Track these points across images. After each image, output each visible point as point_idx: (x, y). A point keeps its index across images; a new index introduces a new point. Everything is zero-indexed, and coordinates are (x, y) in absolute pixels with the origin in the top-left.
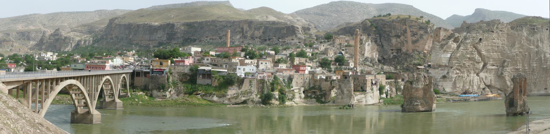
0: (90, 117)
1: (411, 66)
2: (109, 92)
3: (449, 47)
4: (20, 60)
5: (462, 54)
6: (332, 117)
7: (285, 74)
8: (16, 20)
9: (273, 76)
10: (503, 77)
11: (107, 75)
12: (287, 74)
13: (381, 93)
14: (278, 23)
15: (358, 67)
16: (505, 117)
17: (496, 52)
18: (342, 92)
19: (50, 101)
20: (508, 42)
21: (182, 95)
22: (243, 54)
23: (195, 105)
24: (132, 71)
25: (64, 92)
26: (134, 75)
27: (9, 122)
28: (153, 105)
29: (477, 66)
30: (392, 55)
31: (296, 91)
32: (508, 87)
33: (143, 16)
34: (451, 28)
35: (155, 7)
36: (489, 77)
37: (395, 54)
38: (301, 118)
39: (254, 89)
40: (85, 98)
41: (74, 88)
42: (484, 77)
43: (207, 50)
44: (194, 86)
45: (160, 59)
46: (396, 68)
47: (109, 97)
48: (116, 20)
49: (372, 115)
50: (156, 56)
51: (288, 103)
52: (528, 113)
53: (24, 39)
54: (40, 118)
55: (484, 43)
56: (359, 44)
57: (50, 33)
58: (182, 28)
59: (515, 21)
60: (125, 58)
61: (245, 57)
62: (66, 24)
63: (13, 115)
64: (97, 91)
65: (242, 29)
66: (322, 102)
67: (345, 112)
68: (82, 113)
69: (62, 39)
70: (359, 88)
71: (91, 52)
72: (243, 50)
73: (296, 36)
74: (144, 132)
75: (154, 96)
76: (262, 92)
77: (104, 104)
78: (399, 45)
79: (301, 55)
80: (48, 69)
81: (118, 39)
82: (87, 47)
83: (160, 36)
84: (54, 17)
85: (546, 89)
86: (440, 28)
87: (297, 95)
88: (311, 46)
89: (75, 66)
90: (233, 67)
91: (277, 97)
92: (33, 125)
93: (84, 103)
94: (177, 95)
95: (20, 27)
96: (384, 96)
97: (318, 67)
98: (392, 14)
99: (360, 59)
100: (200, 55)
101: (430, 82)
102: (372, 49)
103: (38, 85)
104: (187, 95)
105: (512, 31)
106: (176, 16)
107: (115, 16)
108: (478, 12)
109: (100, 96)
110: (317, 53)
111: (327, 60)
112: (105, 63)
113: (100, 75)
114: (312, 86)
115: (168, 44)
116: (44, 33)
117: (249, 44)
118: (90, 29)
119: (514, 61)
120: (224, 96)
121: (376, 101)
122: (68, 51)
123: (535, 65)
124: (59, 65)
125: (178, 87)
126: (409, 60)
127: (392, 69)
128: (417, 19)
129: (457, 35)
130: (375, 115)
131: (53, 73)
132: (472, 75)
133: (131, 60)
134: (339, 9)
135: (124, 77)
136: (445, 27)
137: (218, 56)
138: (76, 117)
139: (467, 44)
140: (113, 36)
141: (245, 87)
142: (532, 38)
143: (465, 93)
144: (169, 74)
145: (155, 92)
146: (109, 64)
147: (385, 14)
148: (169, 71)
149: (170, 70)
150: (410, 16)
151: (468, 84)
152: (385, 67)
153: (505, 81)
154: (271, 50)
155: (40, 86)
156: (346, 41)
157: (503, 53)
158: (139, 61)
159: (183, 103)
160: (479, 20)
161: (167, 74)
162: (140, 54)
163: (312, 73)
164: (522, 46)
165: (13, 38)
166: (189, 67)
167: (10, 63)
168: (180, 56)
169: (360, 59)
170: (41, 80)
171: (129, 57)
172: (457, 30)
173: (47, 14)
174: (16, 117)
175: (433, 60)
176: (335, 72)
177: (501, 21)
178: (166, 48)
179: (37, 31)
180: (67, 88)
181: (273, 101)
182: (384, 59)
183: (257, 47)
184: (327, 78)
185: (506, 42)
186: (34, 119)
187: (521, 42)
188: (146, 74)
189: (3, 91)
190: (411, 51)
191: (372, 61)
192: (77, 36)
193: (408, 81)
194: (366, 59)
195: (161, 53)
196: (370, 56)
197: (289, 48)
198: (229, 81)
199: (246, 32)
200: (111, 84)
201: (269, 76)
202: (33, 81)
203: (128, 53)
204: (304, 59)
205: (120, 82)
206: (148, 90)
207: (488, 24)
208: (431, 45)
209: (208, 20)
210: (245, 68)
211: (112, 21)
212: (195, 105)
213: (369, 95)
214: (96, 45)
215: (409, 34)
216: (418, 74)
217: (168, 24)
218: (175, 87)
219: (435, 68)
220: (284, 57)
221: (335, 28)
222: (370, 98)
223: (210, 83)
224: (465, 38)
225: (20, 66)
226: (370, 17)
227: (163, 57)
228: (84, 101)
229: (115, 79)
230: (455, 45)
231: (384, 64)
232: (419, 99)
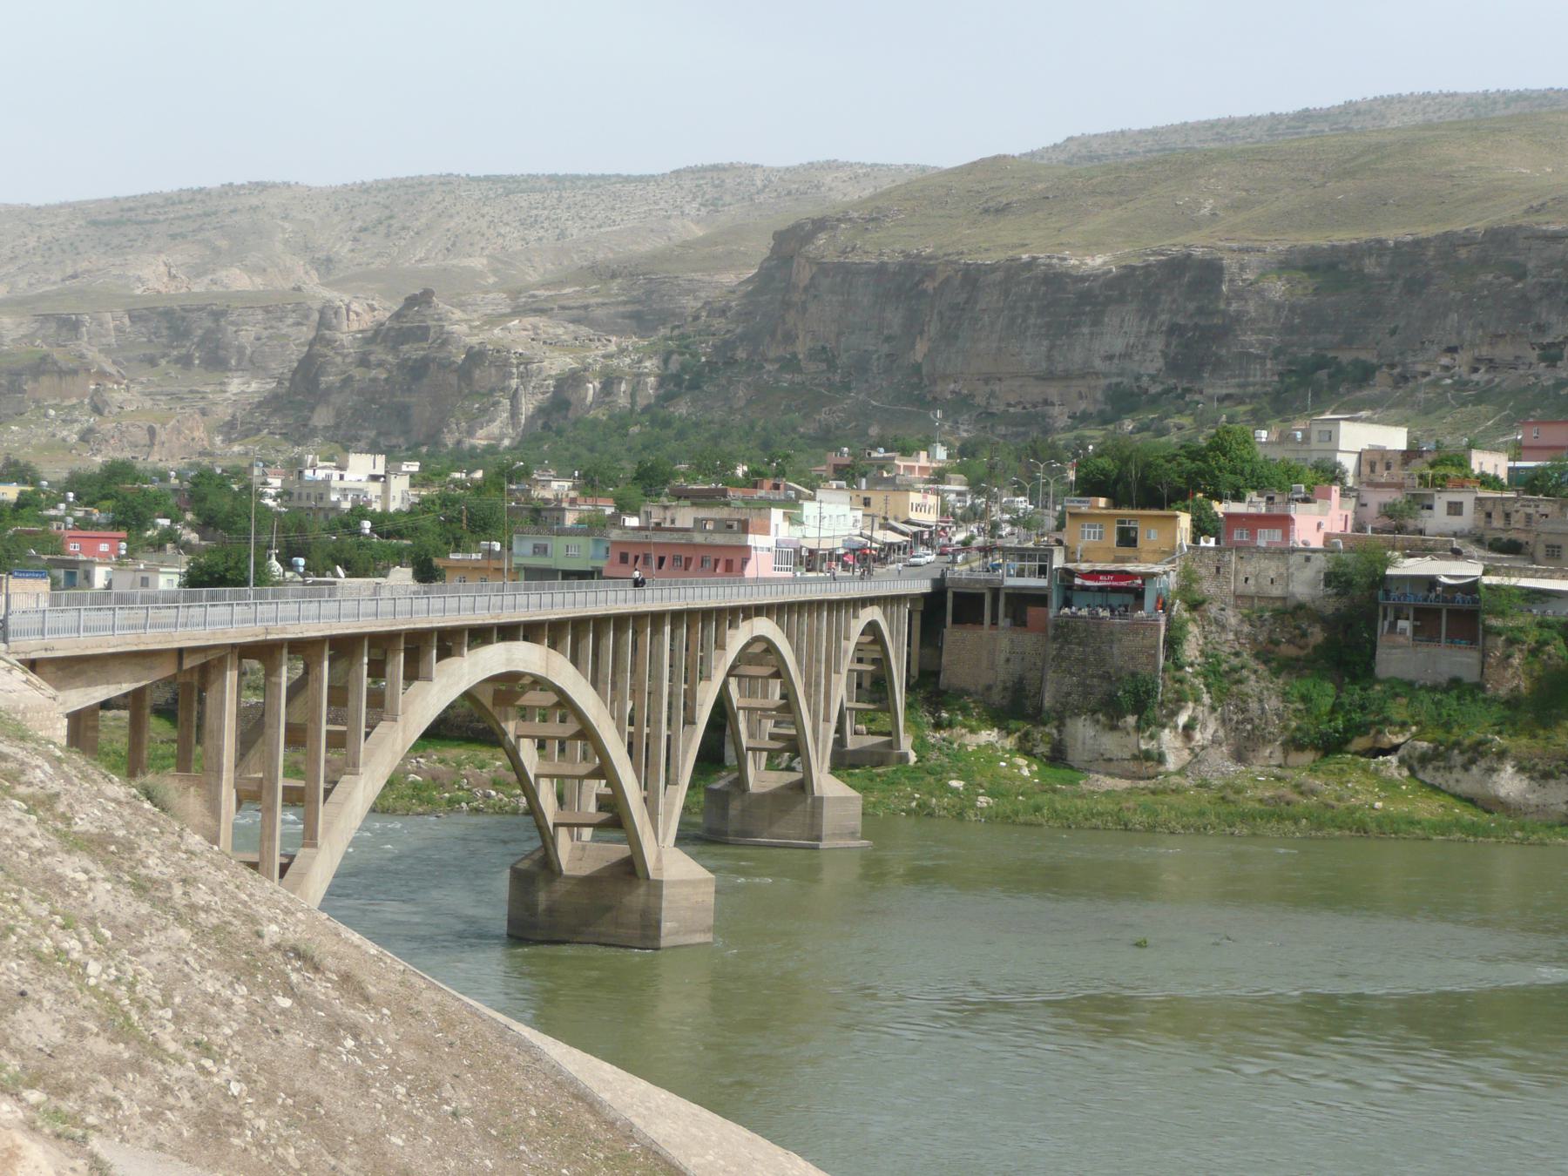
0: (637, 898)
2: (769, 726)
4: (155, 503)
8: (125, 222)
19: (362, 790)
21: (1270, 754)
23: (1362, 829)
24: (925, 587)
25: (464, 726)
26: (939, 611)
27: (71, 944)
28: (1067, 822)
33: (1002, 210)
35: (1084, 141)
40: (605, 770)
41: (533, 698)
44: (1355, 694)
45: (1116, 502)
47: (771, 766)
48: (822, 239)
50: (1090, 486)
53: (185, 362)
54: (297, 908)
57: (367, 321)
58: (1277, 288)
60: (877, 498)
62: (478, 263)
63: (103, 894)
64: (690, 721)
68: (586, 869)
69: (446, 365)
71: (650, 458)
74: (1007, 1007)
75: (1076, 755)
77: (735, 807)
80: (352, 571)
81: (831, 364)
82: (620, 423)
83: (1119, 345)
84: (392, 206)
89: (541, 550)
92: (246, 958)
93: (603, 803)
94: (1239, 756)
95: (154, 275)
100: (1398, 473)
103: (284, 677)
104: (1308, 757)
106: (1236, 207)
107: (816, 213)
109: (711, 756)
112: (745, 527)
113: (706, 614)
115: (1178, 399)
116: (323, 323)
118: (640, 297)
122: (491, 450)
124: (430, 541)
125: (1243, 698)
131: (389, 601)
133: (923, 508)
135: (872, 627)
137: (1529, 483)
138: (542, 899)
140: (802, 347)
144: (1178, 607)
145: (1083, 733)
146: (771, 538)
148: (1184, 590)
149: (1188, 578)
155: (296, 689)
158: (972, 515)
159: (1277, 811)
161: (1164, 605)
165: (107, 350)
166: (1320, 563)
167: (84, 524)
168: (1258, 487)
170: (301, 648)
171: (908, 487)
173: (348, 189)
174: (128, 907)
178: (1162, 432)
179: (273, 309)
180: (487, 699)
186: (252, 919)
188: (1022, 604)
189: (32, 724)
192: (554, 343)
195: (1125, 461)
200: (780, 673)
202: (246, 651)
203: (901, 462)
205: (847, 663)
209: (1458, 226)
211: (790, 243)
214: (681, 409)
217: (1178, 266)
218: (1221, 697)
223: (1470, 676)
227: (1138, 488)
228: (599, 786)
229: (814, 637)
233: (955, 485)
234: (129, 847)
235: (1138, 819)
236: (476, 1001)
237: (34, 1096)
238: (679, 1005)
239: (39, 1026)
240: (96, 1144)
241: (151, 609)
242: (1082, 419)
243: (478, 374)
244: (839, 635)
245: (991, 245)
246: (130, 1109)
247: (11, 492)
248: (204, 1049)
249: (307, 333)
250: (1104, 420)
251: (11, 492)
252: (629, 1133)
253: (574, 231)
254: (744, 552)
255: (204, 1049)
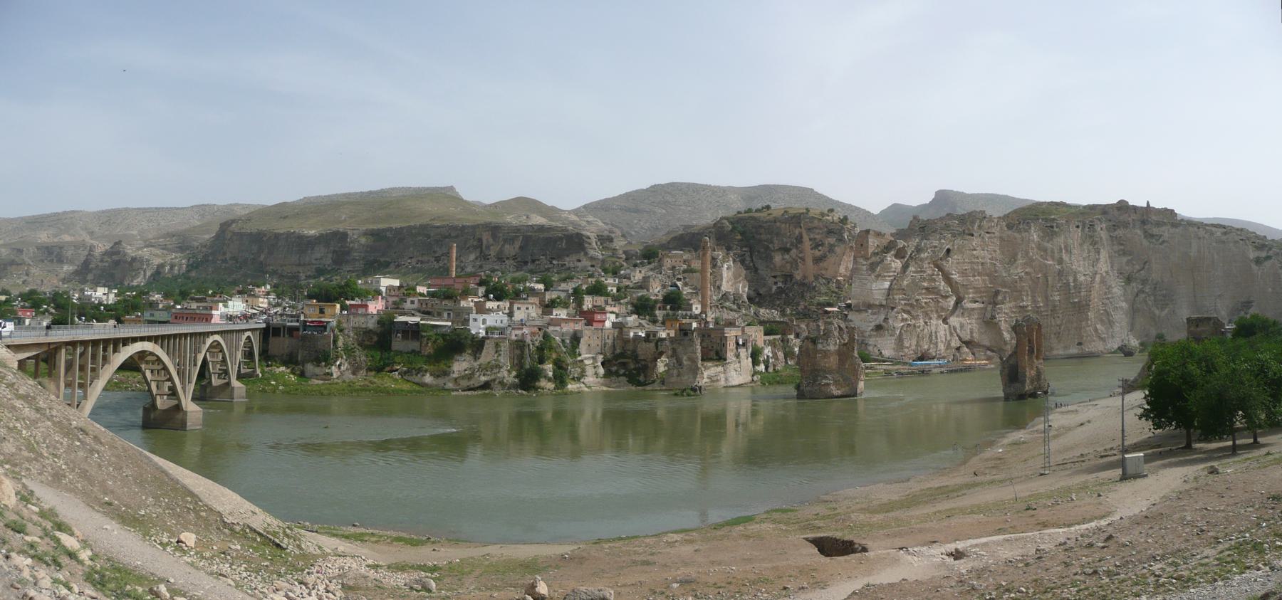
0: (180, 416)
1: (814, 308)
3: (887, 268)
5: (913, 281)
6: (661, 413)
7: (564, 330)
8: (37, 222)
9: (541, 334)
10: (996, 324)
11: (215, 333)
12: (569, 328)
13: (755, 362)
14: (550, 229)
15: (709, 313)
16: (1001, 404)
17: (980, 274)
18: (680, 362)
19: (100, 384)
20: (1003, 253)
21: (363, 372)
22: (481, 290)
23: (388, 393)
24: (264, 326)
25: (130, 366)
26: (269, 332)
29: (943, 303)
30: (774, 288)
31: (587, 362)
32: (1006, 343)
33: (285, 217)
34: (889, 230)
35: (309, 198)
36: (966, 325)
37: (780, 284)
38: (599, 415)
39: (505, 361)
40: (170, 379)
42: (958, 326)
43: (412, 283)
46: (783, 313)
49: (738, 407)
50: (310, 297)
51: (571, 387)
52: (1046, 393)
53: (52, 261)
54: (81, 417)
55: (956, 257)
56: (709, 266)
57: (103, 249)
58: (363, 240)
59: (1015, 212)
60: (250, 300)
61: (486, 296)
62: (135, 232)
63: (26, 411)
65: (480, 240)
66: (639, 384)
67: (684, 402)
68: (165, 407)
69: (126, 262)
70: (712, 354)
72: (481, 284)
73: (586, 254)
75: (307, 374)
76: (521, 365)
78: (788, 266)
79: (598, 290)
82: (175, 278)
83: (319, 256)
84: (110, 217)
85: (1080, 344)
86: (868, 232)
87: (590, 371)
88: (615, 273)
89: (152, 315)
90: (462, 317)
91: (551, 374)
92: (67, 431)
93: (170, 389)
94: (354, 373)
95: (44, 237)
96: (762, 367)
97: (629, 314)
98: (773, 206)
99: (713, 297)
101: (852, 339)
102: (736, 276)
103: (78, 351)
105: (1010, 232)
106: (351, 217)
107: (232, 217)
108: (942, 197)
109: (202, 375)
110: (627, 287)
111: (648, 300)
112: (211, 308)
113: (200, 334)
114: (618, 351)
117: (493, 271)
118: (182, 243)
119: (1016, 293)
120: (446, 374)
121: (745, 378)
123: (1057, 298)
126: (808, 295)
127: (775, 315)
128: (823, 214)
129: (901, 243)
130: (746, 406)
132: (934, 322)
134: (669, 198)
135: (249, 338)
136: (878, 229)
139: (922, 260)
140: (228, 256)
141: (487, 355)
142: (1049, 245)
143: (921, 358)
145: (310, 368)
146: (219, 311)
147: (759, 206)
148: (338, 326)
149: (339, 322)
150: (807, 210)
151: (926, 340)
152: (762, 311)
153: (999, 332)
154: (537, 282)
155: (82, 355)
156: (685, 262)
157: (993, 276)
158: (278, 305)
159: (364, 389)
160: (943, 214)
162: (279, 291)
163: (619, 326)
164: (1030, 262)
166: (376, 318)
167: (23, 307)
169: (713, 297)
170: (84, 343)
172: (901, 234)
174: (34, 415)
175: (855, 294)
176: (663, 323)
177: (988, 213)
179: (76, 246)
181: (543, 383)
182: (759, 294)
183: (509, 277)
184: (648, 335)
185: (998, 254)
187: (1027, 253)
188: (292, 331)
189: (8, 363)
190: (812, 279)
191: (736, 298)
192: (156, 255)
193: (807, 338)
194: (725, 297)
196: (731, 290)
197: (571, 278)
198: (457, 344)
199: (488, 247)
200: (222, 351)
201: (533, 334)
202: (67, 343)
204: (603, 298)
206: (296, 363)
207: (963, 219)
208: (850, 266)
210: (486, 319)
211: (225, 226)
212: (388, 392)
213: (731, 367)
214: (193, 274)
215: (807, 244)
216: (826, 323)
217: (335, 234)
218: (349, 356)
219: (859, 311)
220: (563, 295)
221: (661, 236)
222: (733, 373)
224: (919, 250)
225: (43, 313)
226: (731, 213)
227: (326, 297)
228: (169, 384)
230: (897, 264)
231: (760, 305)
232: (831, 372)
233: (272, 296)
234: (34, 398)
235: (325, 392)
236: (133, 445)
237: (7, 466)
238: (193, 448)
239: (9, 447)
240: (24, 480)
241: (37, 331)
242: (308, 277)
243: (134, 265)
244: (238, 340)
245: (282, 227)
246: (34, 471)
247: (3, 298)
248: (55, 456)
249: (86, 253)
250: (315, 277)
251: (3, 298)
252: (177, 482)
253: (162, 223)
254: (211, 316)
255: (55, 456)
